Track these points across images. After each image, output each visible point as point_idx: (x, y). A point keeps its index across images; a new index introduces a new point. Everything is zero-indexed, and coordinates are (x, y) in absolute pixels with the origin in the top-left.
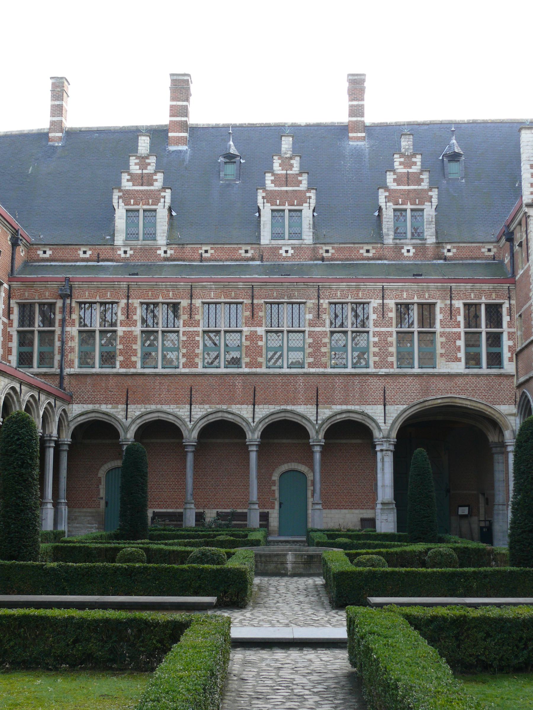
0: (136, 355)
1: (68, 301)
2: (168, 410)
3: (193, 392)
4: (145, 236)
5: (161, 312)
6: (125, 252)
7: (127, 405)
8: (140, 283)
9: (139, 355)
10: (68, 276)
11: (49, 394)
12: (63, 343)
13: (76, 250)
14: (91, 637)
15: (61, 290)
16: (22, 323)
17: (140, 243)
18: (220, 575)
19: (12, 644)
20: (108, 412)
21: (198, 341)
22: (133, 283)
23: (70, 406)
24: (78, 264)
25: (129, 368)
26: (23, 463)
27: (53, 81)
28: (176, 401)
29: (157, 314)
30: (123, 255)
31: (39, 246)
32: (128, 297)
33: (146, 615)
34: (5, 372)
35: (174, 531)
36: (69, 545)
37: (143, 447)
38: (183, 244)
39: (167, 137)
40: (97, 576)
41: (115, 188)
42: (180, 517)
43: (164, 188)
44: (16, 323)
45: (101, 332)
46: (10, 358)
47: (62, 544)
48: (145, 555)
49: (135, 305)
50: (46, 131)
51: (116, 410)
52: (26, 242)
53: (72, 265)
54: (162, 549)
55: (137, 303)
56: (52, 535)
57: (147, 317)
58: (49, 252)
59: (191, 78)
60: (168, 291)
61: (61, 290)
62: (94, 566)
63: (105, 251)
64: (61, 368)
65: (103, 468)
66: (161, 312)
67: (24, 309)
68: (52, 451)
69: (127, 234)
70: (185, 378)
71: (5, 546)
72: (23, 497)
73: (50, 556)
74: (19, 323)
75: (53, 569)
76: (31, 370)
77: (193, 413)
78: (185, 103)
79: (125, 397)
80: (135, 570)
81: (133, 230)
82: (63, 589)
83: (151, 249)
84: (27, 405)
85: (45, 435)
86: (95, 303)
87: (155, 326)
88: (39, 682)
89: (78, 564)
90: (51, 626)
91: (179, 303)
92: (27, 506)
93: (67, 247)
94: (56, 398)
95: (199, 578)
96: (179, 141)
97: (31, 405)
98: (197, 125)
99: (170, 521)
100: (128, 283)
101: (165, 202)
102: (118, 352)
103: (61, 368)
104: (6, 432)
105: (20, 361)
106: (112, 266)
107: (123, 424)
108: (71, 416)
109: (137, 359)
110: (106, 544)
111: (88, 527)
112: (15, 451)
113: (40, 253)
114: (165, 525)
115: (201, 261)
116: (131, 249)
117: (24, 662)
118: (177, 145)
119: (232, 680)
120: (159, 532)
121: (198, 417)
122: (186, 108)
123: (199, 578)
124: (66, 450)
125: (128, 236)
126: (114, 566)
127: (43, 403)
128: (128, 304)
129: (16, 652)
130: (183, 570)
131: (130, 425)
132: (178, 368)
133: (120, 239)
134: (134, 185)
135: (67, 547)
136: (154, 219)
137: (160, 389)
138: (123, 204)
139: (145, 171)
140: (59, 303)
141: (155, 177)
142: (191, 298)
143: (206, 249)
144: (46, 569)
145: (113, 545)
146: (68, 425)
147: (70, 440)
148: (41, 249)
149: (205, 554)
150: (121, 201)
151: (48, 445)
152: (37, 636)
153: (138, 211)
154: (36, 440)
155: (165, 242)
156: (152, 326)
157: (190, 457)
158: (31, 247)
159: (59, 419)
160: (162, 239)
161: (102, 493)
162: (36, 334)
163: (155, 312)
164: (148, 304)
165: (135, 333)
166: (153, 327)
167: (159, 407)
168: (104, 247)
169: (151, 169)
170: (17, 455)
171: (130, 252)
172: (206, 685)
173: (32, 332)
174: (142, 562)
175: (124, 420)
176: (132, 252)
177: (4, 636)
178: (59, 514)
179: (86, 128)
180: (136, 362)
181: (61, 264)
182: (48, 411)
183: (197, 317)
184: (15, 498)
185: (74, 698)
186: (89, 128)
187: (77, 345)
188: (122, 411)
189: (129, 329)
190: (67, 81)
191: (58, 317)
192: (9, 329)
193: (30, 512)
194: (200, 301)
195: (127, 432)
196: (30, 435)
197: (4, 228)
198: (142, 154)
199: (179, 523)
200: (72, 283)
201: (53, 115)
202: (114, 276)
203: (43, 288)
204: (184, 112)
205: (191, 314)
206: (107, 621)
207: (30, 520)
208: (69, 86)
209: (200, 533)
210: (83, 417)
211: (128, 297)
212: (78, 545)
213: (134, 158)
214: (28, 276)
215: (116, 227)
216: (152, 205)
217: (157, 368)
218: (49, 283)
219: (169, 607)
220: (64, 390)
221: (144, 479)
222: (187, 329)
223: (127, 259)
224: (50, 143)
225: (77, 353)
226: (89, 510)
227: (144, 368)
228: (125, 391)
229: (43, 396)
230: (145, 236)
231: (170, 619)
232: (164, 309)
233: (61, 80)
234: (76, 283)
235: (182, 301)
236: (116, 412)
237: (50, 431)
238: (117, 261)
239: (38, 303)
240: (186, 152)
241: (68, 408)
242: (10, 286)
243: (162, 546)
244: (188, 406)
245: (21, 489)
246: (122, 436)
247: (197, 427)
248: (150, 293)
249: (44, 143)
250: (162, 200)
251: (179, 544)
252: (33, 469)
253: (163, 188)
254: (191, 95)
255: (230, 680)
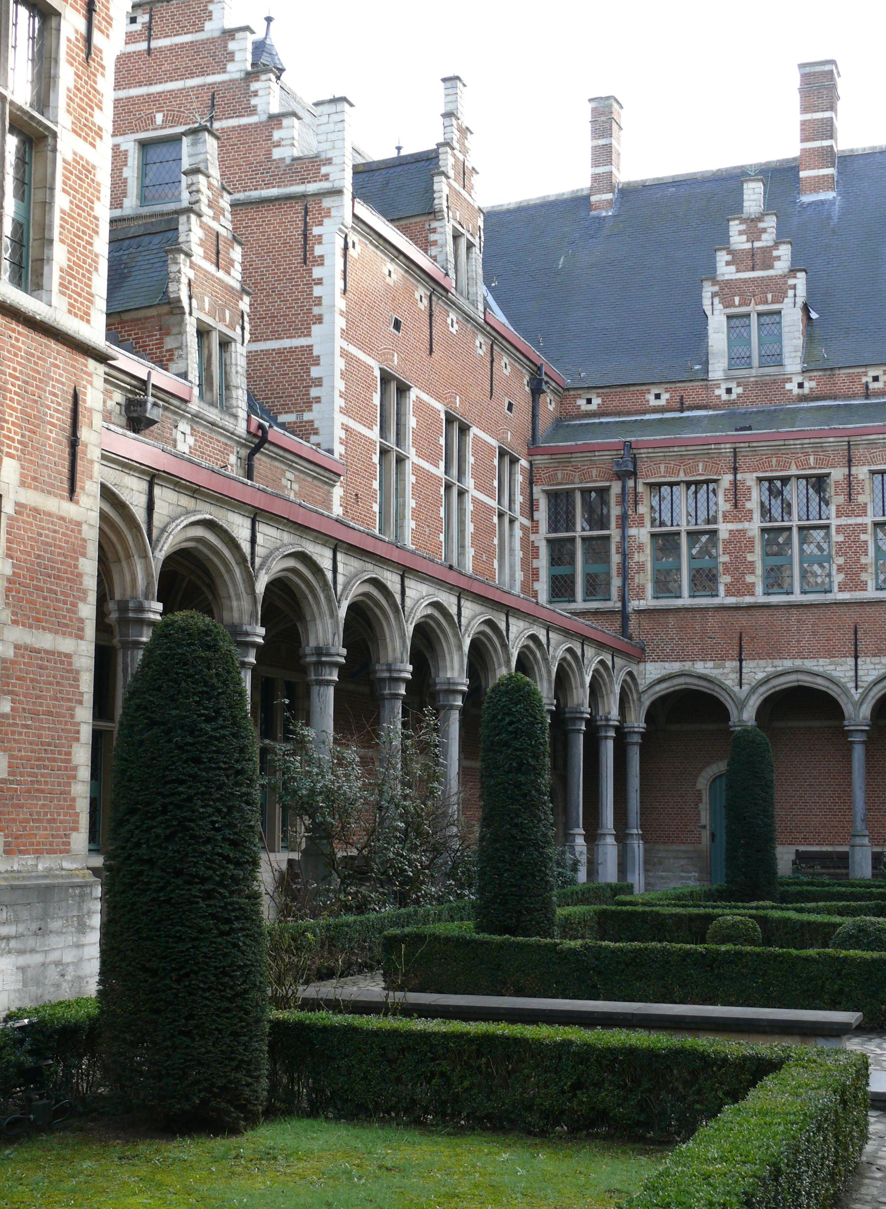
0: (753, 573)
1: (631, 483)
2: (816, 668)
3: (859, 634)
4: (763, 360)
5: (795, 493)
6: (729, 391)
7: (741, 661)
8: (755, 444)
9: (759, 571)
10: (628, 439)
11: (601, 646)
12: (624, 556)
13: (643, 393)
14: (604, 1080)
15: (618, 464)
16: (554, 526)
17: (753, 372)
18: (879, 970)
19: (466, 1084)
20: (706, 675)
21: (866, 542)
22: (742, 445)
23: (642, 665)
24: (647, 417)
25: (741, 596)
26: (521, 765)
27: (594, 104)
28: (829, 651)
29: (788, 497)
30: (725, 397)
31: (580, 392)
32: (735, 470)
33: (704, 1042)
34: (518, 610)
35: (828, 885)
36: (624, 908)
37: (763, 734)
38: (832, 369)
39: (798, 179)
40: (651, 967)
41: (706, 279)
42: (843, 860)
43: (793, 271)
44: (543, 526)
45: (689, 533)
46: (537, 586)
47: (613, 908)
48: (759, 929)
49: (748, 483)
50: (585, 193)
51: (721, 671)
52: (557, 387)
53: (636, 420)
54: (789, 919)
55: (752, 480)
56: (609, 890)
57: (770, 504)
58: (596, 401)
59: (837, 67)
60: (807, 454)
61: (618, 464)
62: (646, 949)
63: (693, 392)
64: (623, 600)
65: (703, 774)
66: (795, 493)
67: (556, 501)
68: (610, 744)
69: (731, 359)
70: (844, 609)
71: (494, 910)
72: (522, 823)
73: (591, 928)
74: (550, 526)
75: (573, 951)
76: (572, 606)
77: (860, 673)
78: (827, 114)
79: (737, 648)
80: (720, 958)
81: (740, 350)
82: (594, 987)
83: (774, 382)
84: (560, 666)
85: (598, 718)
86: (677, 483)
87: (786, 518)
88: (505, 1156)
89: (617, 944)
90: (532, 1057)
91: (828, 475)
92: (531, 840)
93: (627, 389)
94: (615, 652)
95: (839, 975)
96: (819, 184)
97: (569, 665)
98: (852, 150)
99: (823, 867)
100: (733, 446)
101: (795, 296)
102: (721, 568)
103: (623, 600)
104: (490, 711)
105: (553, 590)
106: (705, 416)
107: (735, 694)
108: (643, 684)
109: (756, 579)
110: (691, 909)
111: (682, 878)
112: (507, 744)
113: (582, 402)
114: (813, 875)
115: (867, 397)
116: (739, 385)
117: (489, 1117)
118: (815, 191)
119: (872, 1178)
120: (799, 888)
121: (870, 679)
122: (830, 123)
123: (839, 975)
124: (636, 743)
125: (733, 362)
126: (680, 949)
127: (591, 661)
128: (735, 483)
129: (474, 1100)
130: (807, 960)
131: (748, 697)
132: (830, 592)
133: (718, 369)
134: (738, 271)
135: (621, 912)
136: (778, 327)
137: (799, 630)
138: (721, 306)
139: (757, 244)
140: (616, 488)
141: (775, 253)
142: (850, 463)
143: (875, 374)
144: (562, 951)
145: (702, 911)
146: (639, 699)
147: (643, 725)
148: (583, 396)
149: (863, 930)
150: (716, 300)
151: (603, 734)
152: (509, 1073)
153: (748, 315)
154: (542, 723)
155: (798, 368)
156: (780, 519)
157: (858, 753)
158: (566, 393)
159: (622, 688)
160: (793, 363)
161: (705, 818)
162: (579, 542)
163: (785, 493)
164: (770, 480)
165: (750, 534)
166: (783, 521)
167: (798, 663)
168: (690, 384)
169: (767, 239)
170: (509, 751)
171: (737, 391)
172: (753, 1196)
173: (572, 540)
174: (753, 942)
175: (736, 689)
176: (740, 390)
177: (453, 1070)
178: (629, 855)
179: (654, 179)
180: (753, 584)
181: (617, 419)
182: (601, 676)
183: (861, 499)
184: (508, 827)
185: (559, 1192)
186: (658, 179)
187: (649, 559)
188: (733, 671)
189: (740, 526)
190: (618, 102)
191: (615, 511)
192: (532, 537)
193: (536, 850)
194: (865, 469)
195: (742, 709)
196: (531, 715)
197: (516, 364)
198: (750, 214)
199: (844, 871)
200: (635, 451)
201: (596, 163)
202: (709, 434)
203: (588, 463)
204: (827, 130)
205: (850, 494)
206: (631, 1052)
207: (536, 864)
208: (622, 111)
209: (874, 890)
210: (664, 685)
211: (735, 470)
212: (640, 909)
213: (737, 222)
214: (560, 444)
215: (710, 349)
216: (773, 302)
217: (792, 593)
218: (597, 454)
219: (768, 1029)
220: (631, 638)
221: (767, 793)
222: (843, 521)
223: (733, 403)
224: (593, 213)
225: (649, 573)
226: (683, 847)
227: (769, 594)
228: (737, 636)
229: (590, 649)
230: (763, 360)
231: (748, 1052)
232: (801, 487)
233: (607, 102)
234: (642, 451)
235: (832, 471)
236: (722, 674)
237: (607, 710)
238: (714, 408)
239: (579, 488)
240: (832, 202)
241: (638, 670)
242: (531, 462)
243: (792, 915)
244: (851, 661)
245: (520, 810)
246: (734, 717)
247: (869, 698)
248: (774, 460)
249: (583, 214)
250: (791, 293)
251: (829, 912)
252: (539, 774)
253: (791, 271)
254: (838, 98)
255: (867, 1178)
